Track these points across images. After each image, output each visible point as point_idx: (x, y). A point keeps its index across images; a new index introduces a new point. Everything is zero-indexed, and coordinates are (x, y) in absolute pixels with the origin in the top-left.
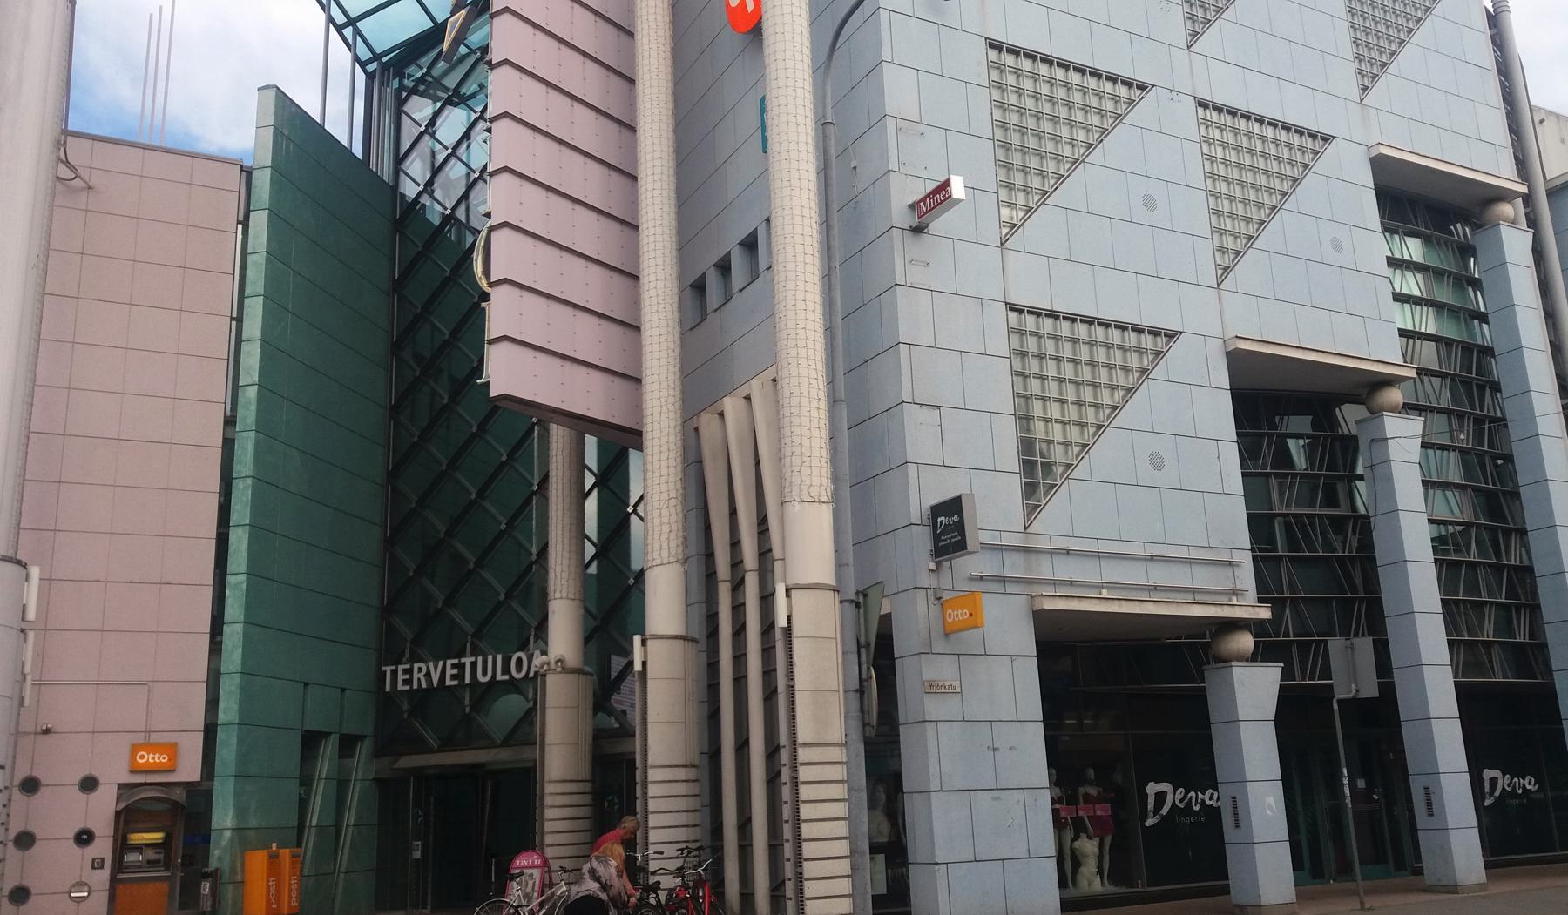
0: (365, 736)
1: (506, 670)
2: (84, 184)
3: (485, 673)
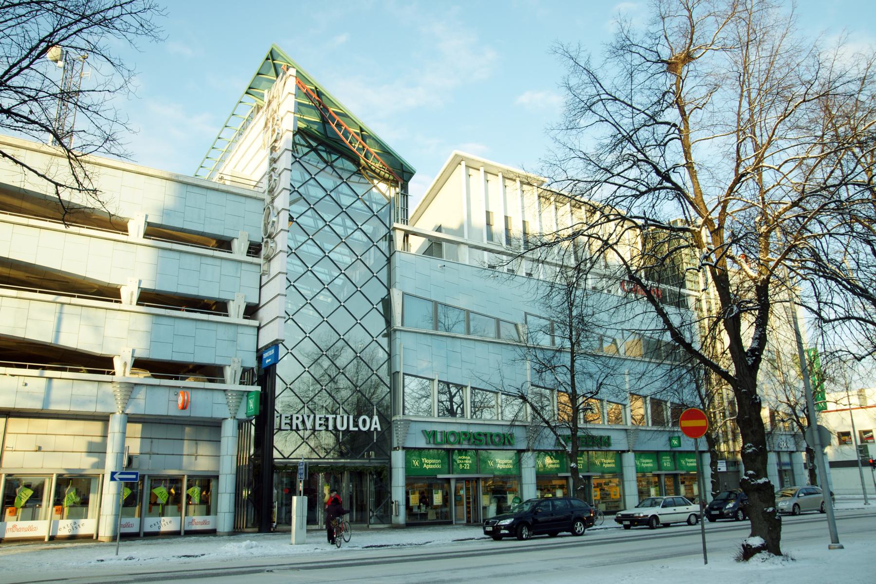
1: (356, 424)
3: (343, 426)
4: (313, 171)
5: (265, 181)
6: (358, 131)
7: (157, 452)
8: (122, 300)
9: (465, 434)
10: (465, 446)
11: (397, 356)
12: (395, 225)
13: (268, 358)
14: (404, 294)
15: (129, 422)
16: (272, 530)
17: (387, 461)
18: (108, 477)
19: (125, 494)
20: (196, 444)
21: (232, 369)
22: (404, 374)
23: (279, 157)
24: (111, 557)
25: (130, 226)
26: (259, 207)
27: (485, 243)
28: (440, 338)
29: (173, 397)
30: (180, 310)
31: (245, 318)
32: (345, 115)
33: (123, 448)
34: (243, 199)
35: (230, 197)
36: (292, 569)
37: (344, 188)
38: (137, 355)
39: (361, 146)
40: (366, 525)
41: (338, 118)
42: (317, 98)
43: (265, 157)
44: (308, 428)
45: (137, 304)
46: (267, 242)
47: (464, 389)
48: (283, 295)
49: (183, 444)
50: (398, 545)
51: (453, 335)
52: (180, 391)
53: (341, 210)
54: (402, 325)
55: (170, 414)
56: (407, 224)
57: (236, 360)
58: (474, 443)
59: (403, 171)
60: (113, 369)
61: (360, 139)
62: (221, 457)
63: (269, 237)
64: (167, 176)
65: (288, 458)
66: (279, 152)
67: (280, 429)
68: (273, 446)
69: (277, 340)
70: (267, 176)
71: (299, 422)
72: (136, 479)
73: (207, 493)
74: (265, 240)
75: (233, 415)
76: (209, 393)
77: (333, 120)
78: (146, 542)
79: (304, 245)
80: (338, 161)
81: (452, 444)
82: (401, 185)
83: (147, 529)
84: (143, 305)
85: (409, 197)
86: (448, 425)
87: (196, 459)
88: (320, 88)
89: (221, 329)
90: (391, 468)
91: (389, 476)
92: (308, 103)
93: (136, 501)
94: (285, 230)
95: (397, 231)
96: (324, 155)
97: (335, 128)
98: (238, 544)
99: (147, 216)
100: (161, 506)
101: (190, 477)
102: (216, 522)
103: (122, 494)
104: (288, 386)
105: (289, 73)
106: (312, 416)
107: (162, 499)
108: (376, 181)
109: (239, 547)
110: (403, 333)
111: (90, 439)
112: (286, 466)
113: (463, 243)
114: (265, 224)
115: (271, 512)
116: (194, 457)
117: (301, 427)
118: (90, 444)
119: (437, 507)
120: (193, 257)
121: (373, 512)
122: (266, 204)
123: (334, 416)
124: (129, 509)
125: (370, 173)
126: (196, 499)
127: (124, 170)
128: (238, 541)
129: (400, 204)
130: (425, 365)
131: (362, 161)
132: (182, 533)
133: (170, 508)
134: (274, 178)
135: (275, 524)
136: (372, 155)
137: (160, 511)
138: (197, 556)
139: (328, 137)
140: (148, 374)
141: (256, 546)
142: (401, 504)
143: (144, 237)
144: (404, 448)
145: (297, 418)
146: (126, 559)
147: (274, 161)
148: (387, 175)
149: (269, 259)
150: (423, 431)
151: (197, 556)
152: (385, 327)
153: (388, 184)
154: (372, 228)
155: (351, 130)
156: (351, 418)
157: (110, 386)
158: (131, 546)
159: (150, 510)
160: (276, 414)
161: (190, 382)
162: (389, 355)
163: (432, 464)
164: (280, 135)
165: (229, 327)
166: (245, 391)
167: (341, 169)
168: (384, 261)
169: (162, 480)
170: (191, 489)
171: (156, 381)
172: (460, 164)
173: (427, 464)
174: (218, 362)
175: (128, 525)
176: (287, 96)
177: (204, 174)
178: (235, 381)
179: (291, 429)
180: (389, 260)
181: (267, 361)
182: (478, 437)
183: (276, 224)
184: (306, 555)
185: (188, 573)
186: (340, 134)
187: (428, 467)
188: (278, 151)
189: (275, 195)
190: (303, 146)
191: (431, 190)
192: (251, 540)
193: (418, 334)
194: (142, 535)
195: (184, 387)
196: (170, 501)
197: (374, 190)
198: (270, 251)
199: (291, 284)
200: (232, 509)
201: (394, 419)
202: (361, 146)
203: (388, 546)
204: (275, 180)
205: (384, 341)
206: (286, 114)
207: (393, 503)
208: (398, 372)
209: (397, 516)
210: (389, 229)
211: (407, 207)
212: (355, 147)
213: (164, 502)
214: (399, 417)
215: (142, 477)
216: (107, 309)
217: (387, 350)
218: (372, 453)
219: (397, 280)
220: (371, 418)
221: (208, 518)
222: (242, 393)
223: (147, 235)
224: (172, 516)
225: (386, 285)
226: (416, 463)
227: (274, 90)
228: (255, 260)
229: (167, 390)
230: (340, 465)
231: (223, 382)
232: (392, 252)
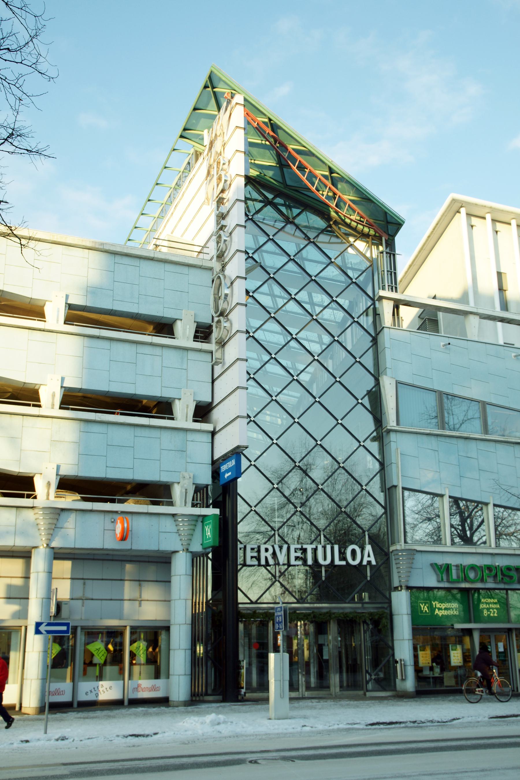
0: (52, 740)
1: (343, 557)
2: (384, 516)
3: (325, 559)
4: (271, 231)
5: (212, 245)
6: (327, 173)
7: (90, 597)
8: (42, 403)
9: (489, 568)
10: (491, 585)
11: (394, 466)
12: (382, 293)
13: (227, 471)
14: (398, 383)
15: (55, 558)
16: (240, 698)
17: (386, 605)
18: (31, 629)
19: (54, 652)
20: (140, 585)
21: (182, 487)
22: (404, 489)
23: (228, 212)
24: (38, 737)
25: (48, 310)
26: (207, 277)
27: (498, 312)
28: (448, 440)
29: (109, 526)
30: (113, 413)
31: (195, 421)
32: (309, 153)
33: (49, 592)
34: (185, 270)
35: (168, 267)
36: (284, 758)
37: (311, 252)
38: (63, 472)
39: (331, 194)
40: (361, 693)
41: (299, 158)
42: (272, 133)
43: (210, 215)
44: (281, 563)
45: (61, 408)
46: (219, 322)
47: (484, 508)
48: (243, 388)
49: (123, 586)
50: (414, 722)
51: (465, 435)
52: (117, 517)
53: (269, 316)
54: (398, 424)
55: (106, 547)
56: (396, 291)
57: (187, 475)
58: (502, 581)
59: (388, 223)
60: (34, 491)
61: (329, 183)
62: (172, 602)
63: (222, 314)
64: (89, 244)
65: (256, 603)
66: (228, 205)
67: (244, 565)
68: (237, 588)
69: (238, 447)
70: (214, 238)
71: (269, 555)
72: (67, 632)
73: (154, 649)
74: (216, 319)
75: (185, 547)
76: (154, 519)
77: (294, 160)
78: (80, 715)
79: (259, 331)
80: (301, 216)
81: (472, 582)
82: (386, 240)
83: (82, 697)
84: (68, 409)
85: (397, 257)
86: (465, 556)
87: (140, 605)
88: (275, 120)
89: (166, 436)
90: (391, 615)
91: (389, 626)
92: (260, 142)
93: (67, 662)
94: (242, 304)
95: (384, 300)
96: (283, 209)
97: (296, 170)
98: (201, 719)
99: (67, 297)
100: (98, 667)
101: (134, 630)
102: (168, 688)
103: (49, 651)
104: (253, 508)
105: (234, 101)
106: (285, 547)
107: (99, 658)
108: (351, 239)
109: (202, 723)
110: (399, 435)
111: (8, 581)
112: (254, 613)
113: (471, 313)
114: (215, 298)
115: (238, 675)
116: (137, 603)
117: (271, 561)
118: (9, 587)
119: (456, 668)
120: (127, 346)
121: (371, 675)
122: (215, 273)
123: (314, 546)
124: (58, 671)
125: (344, 229)
126: (142, 658)
127: (23, 415)
128: (199, 714)
129: (384, 264)
130: (430, 475)
131: (333, 214)
132: (126, 703)
133: (109, 669)
134: (224, 238)
135: (243, 691)
136: (345, 203)
137: (97, 673)
138: (148, 736)
139: (287, 186)
140: (78, 497)
141: (225, 722)
142: (408, 663)
143: (65, 323)
144: (408, 588)
145: (267, 550)
146: (57, 740)
147: (222, 216)
148: (366, 230)
149: (222, 344)
150: (432, 565)
151: (148, 736)
152: (373, 428)
153: (367, 242)
154: (347, 302)
155: (318, 172)
156: (336, 547)
157: (30, 512)
158: (62, 720)
159: (85, 673)
160: (240, 546)
161: (130, 506)
162: (382, 464)
163: (446, 609)
164: (228, 183)
165: (175, 433)
166: (199, 516)
167: (306, 227)
168: (367, 341)
169: (98, 633)
170: (135, 645)
171: (88, 505)
172: (458, 212)
173: (439, 609)
174: (164, 478)
175: (58, 692)
176: (234, 132)
177: (139, 238)
178: (186, 502)
179: (259, 565)
180: (375, 341)
181: (227, 475)
182: (506, 573)
183: (229, 298)
184: (292, 734)
185: (141, 764)
186: (304, 178)
187: (440, 613)
188: (227, 205)
189: (226, 260)
190: (255, 200)
191: (420, 252)
192: (218, 713)
193: (419, 436)
194: (75, 705)
195: (123, 512)
196: (108, 660)
197: (350, 250)
198: (223, 333)
199: (251, 377)
200: (189, 671)
201: (392, 548)
202: (331, 194)
203: (400, 723)
204: (225, 241)
205: (374, 447)
206: (234, 154)
207: (397, 662)
208: (395, 487)
209: (403, 680)
210: (373, 299)
211: (395, 269)
212: (324, 195)
213: (102, 662)
214: (400, 546)
215: (75, 628)
216: (23, 415)
217: (378, 457)
218: (365, 595)
219: (388, 365)
220: (363, 549)
221: (160, 683)
222: (195, 518)
223: (68, 320)
224: (111, 679)
225: (372, 372)
226: (425, 608)
227: (217, 127)
228: (205, 346)
229: (101, 516)
230: (325, 611)
231: (171, 504)
232: (378, 330)
